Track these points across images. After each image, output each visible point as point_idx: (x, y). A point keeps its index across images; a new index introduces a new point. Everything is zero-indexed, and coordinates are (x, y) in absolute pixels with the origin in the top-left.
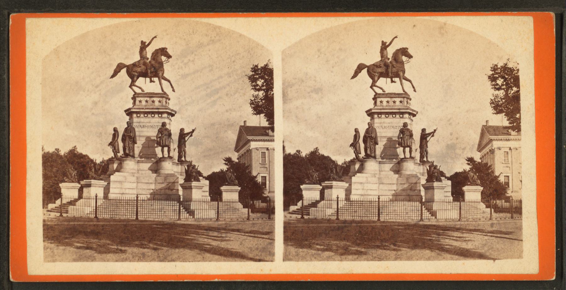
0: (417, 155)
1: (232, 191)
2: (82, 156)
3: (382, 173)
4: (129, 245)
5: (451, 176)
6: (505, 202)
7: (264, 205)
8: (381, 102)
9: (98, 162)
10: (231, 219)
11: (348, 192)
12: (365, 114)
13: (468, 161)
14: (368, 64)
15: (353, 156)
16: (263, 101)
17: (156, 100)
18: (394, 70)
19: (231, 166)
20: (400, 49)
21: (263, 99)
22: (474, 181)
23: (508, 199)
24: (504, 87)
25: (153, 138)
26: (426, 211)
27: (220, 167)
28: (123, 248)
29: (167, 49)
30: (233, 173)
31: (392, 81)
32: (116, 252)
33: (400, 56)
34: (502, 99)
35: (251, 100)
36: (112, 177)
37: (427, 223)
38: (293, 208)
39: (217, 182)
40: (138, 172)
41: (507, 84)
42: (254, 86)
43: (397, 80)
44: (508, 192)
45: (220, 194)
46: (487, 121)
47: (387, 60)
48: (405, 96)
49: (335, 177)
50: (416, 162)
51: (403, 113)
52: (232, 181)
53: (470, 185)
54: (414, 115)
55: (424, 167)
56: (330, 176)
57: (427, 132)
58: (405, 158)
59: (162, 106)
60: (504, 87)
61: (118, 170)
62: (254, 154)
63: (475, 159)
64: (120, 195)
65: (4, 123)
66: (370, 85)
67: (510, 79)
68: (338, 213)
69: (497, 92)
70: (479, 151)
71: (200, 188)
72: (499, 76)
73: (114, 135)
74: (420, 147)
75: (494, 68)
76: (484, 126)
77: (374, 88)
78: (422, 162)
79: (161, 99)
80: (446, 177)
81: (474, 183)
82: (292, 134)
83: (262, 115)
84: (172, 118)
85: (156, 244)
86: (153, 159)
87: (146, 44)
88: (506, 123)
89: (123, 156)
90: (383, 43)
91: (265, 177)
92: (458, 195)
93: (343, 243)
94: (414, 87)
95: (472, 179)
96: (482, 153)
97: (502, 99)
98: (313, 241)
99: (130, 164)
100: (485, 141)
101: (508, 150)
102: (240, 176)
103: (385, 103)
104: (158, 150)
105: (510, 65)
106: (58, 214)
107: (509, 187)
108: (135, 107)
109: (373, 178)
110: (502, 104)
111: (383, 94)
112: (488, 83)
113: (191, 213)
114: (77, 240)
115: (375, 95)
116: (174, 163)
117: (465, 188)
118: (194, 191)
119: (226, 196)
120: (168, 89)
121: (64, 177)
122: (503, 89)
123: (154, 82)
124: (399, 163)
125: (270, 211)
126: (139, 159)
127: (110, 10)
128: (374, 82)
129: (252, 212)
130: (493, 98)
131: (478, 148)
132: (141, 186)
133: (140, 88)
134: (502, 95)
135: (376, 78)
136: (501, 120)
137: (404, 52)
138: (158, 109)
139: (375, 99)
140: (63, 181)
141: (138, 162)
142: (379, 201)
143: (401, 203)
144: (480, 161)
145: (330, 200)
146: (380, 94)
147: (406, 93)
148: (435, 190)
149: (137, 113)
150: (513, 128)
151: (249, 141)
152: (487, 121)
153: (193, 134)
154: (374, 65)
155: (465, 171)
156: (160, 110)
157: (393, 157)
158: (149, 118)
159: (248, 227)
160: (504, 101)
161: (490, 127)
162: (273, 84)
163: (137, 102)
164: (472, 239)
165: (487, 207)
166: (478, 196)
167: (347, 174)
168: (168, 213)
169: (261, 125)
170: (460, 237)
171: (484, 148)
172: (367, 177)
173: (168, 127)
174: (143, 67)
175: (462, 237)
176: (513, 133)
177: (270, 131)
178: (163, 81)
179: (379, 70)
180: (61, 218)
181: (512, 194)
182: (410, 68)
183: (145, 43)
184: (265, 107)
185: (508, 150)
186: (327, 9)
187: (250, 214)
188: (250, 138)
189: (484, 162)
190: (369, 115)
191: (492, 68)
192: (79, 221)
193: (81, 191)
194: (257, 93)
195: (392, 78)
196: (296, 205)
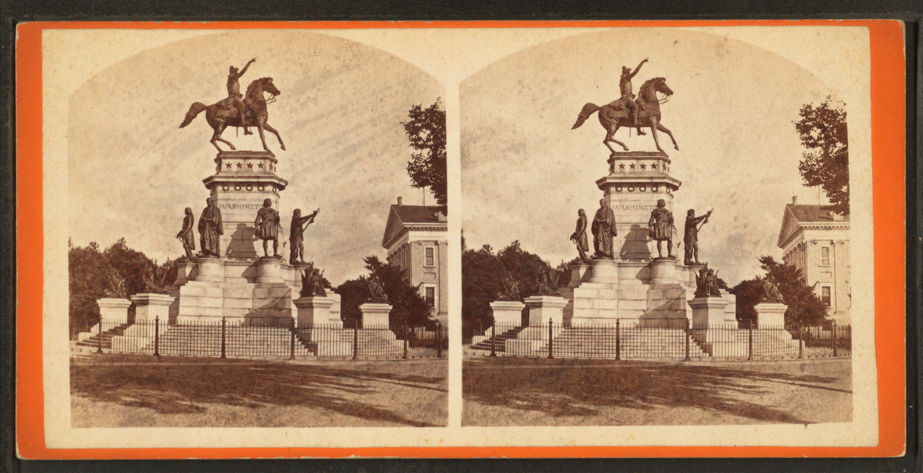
0: (680, 253)
1: (377, 312)
2: (133, 255)
3: (623, 282)
4: (211, 400)
5: (736, 288)
7: (430, 334)
8: (622, 166)
9: (160, 264)
10: (377, 358)
11: (568, 313)
12: (596, 186)
13: (763, 262)
14: (600, 105)
15: (575, 254)
17: (255, 163)
18: (643, 114)
19: (377, 271)
20: (653, 80)
21: (430, 162)
22: (773, 295)
23: (828, 325)
24: (822, 142)
25: (249, 225)
26: (694, 344)
27: (359, 272)
29: (272, 79)
30: (380, 282)
31: (640, 133)
33: (653, 91)
34: (818, 161)
35: (410, 164)
36: (182, 288)
37: (696, 363)
38: (477, 339)
39: (353, 296)
40: (225, 281)
41: (827, 137)
42: (415, 140)
43: (647, 130)
44: (829, 313)
45: (359, 316)
46: (794, 198)
47: (631, 98)
48: (660, 156)
49: (547, 288)
50: (678, 263)
51: (657, 185)
52: (379, 295)
54: (676, 188)
55: (692, 272)
56: (538, 288)
57: (697, 215)
59: (265, 172)
60: (822, 142)
61: (193, 277)
62: (414, 252)
63: (775, 260)
64: (196, 319)
65: (7, 200)
66: (604, 138)
67: (832, 129)
68: (550, 348)
70: (782, 247)
71: (327, 306)
73: (186, 221)
74: (685, 240)
75: (806, 111)
76: (789, 205)
77: (610, 143)
78: (689, 265)
80: (727, 289)
81: (773, 299)
82: (477, 219)
83: (428, 188)
84: (281, 193)
85: (254, 398)
86: (249, 260)
87: (239, 72)
88: (825, 201)
89: (201, 254)
90: (625, 71)
91: (433, 288)
92: (747, 318)
93: (559, 397)
94: (674, 142)
95: (770, 291)
96: (786, 249)
97: (818, 161)
98: (511, 393)
99: (211, 268)
101: (828, 244)
102: (392, 287)
103: (627, 169)
105: (832, 107)
106: (95, 350)
107: (829, 304)
108: (220, 174)
109: (609, 291)
110: (426, 172)
111: (625, 154)
113: (312, 347)
114: (125, 392)
115: (611, 156)
116: (283, 266)
117: (759, 307)
118: (316, 311)
119: (368, 320)
120: (273, 146)
121: (105, 288)
122: (821, 145)
123: (251, 133)
125: (440, 345)
126: (227, 259)
127: (180, 17)
128: (610, 134)
129: (412, 346)
130: (803, 160)
131: (782, 236)
132: (230, 303)
133: (228, 143)
134: (818, 155)
135: (613, 128)
136: (817, 196)
137: (659, 84)
138: (258, 177)
139: (611, 161)
140: (104, 296)
141: (226, 264)
142: (618, 328)
143: (655, 332)
144: (783, 262)
145: (539, 327)
146: (619, 154)
147: (662, 152)
148: (710, 311)
149: (223, 184)
150: (837, 210)
151: (406, 230)
152: (794, 198)
154: (609, 105)
156: (261, 180)
157: (641, 256)
158: (243, 192)
159: (404, 369)
160: (821, 164)
162: (444, 137)
163: (224, 167)
164: (770, 390)
165: (794, 338)
166: (780, 320)
167: (566, 284)
168: (273, 347)
169: (426, 205)
170: (750, 387)
171: (789, 241)
172: (598, 289)
173: (273, 206)
174: (233, 109)
175: (753, 387)
176: (837, 217)
177: (440, 213)
178: (266, 132)
179: (619, 114)
180: (99, 355)
181: (835, 317)
182: (669, 111)
183: (237, 69)
184: (432, 175)
185: (828, 244)
187: (408, 349)
188: (407, 224)
190: (601, 188)
191: (802, 111)
193: (132, 311)
194: (419, 151)
195: (638, 128)
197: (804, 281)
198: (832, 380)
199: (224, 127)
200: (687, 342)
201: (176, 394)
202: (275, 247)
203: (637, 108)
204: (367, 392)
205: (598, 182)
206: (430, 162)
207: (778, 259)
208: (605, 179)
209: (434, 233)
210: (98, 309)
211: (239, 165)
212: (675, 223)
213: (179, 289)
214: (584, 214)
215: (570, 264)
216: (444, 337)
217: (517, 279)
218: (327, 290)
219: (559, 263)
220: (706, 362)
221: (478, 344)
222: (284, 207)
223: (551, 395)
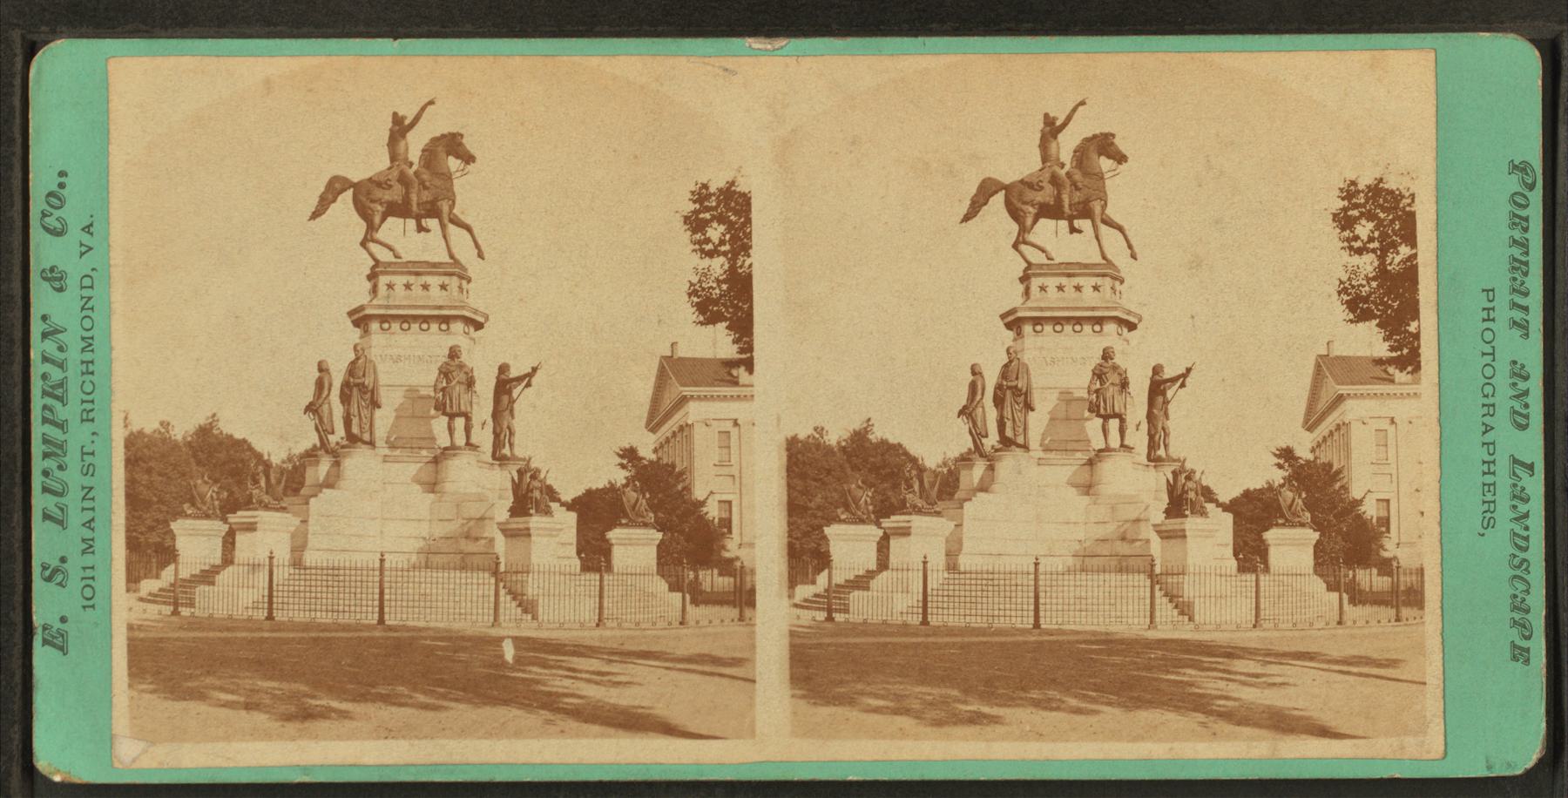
2: (886, 447)
4: (1010, 701)
5: (1234, 502)
6: (720, 574)
7: (724, 583)
8: (390, 286)
9: (276, 460)
11: (299, 547)
12: (1001, 324)
13: (622, 457)
14: (1007, 181)
15: (312, 439)
16: (724, 287)
21: (724, 281)
22: (1295, 514)
23: (1386, 567)
24: (1376, 245)
25: (423, 392)
26: (1165, 600)
27: (1264, 473)
28: (344, 706)
29: (1113, 136)
30: (1298, 491)
32: (975, 719)
34: (1368, 279)
35: (692, 284)
38: (149, 586)
39: (598, 514)
41: (1383, 237)
42: (699, 242)
43: (432, 223)
45: (1262, 551)
47: (1057, 169)
48: (454, 269)
49: (266, 499)
51: (446, 320)
53: (626, 525)
55: (506, 473)
56: (904, 501)
58: (1108, 449)
60: (1376, 245)
61: (984, 488)
67: (1392, 222)
68: (270, 602)
69: (1356, 260)
71: (551, 533)
72: (1362, 214)
75: (1349, 192)
78: (499, 458)
80: (1219, 505)
82: (805, 384)
83: (721, 326)
85: (1084, 697)
86: (424, 453)
87: (407, 122)
88: (1382, 349)
89: (345, 442)
93: (936, 692)
94: (1130, 247)
95: (634, 507)
96: (659, 434)
97: (1368, 279)
98: (859, 686)
99: (358, 463)
100: (667, 402)
101: (728, 426)
102: (659, 500)
104: (439, 425)
105: (1391, 184)
106: (168, 610)
110: (1369, 296)
112: (685, 236)
113: (528, 607)
114: (218, 683)
115: (373, 268)
117: (614, 535)
119: (620, 556)
120: (465, 251)
121: (187, 502)
122: (725, 254)
123: (428, 231)
124: (436, 461)
125: (743, 598)
126: (387, 452)
127: (305, 30)
128: (1023, 230)
130: (695, 280)
131: (1306, 421)
134: (1370, 268)
135: (1029, 221)
136: (1369, 341)
139: (372, 276)
140: (182, 514)
141: (385, 459)
142: (382, 569)
143: (440, 575)
144: (1311, 457)
145: (895, 571)
146: (1041, 266)
147: (456, 262)
150: (1401, 363)
153: (534, 380)
154: (1022, 181)
159: (689, 643)
160: (1374, 284)
162: (749, 236)
163: (382, 289)
164: (1291, 681)
165: (671, 589)
166: (1307, 559)
167: (296, 491)
170: (1257, 676)
171: (668, 415)
173: (464, 358)
175: (608, 673)
176: (1400, 376)
177: (742, 369)
180: (829, 625)
181: (1399, 553)
182: (1123, 191)
184: (729, 302)
185: (728, 426)
186: (906, 26)
187: (689, 608)
189: (1323, 459)
192: (201, 628)
193: (229, 542)
194: (707, 262)
196: (814, 582)
197: (687, 489)
198: (1393, 663)
200: (1152, 597)
201: (955, 693)
202: (468, 430)
203: (1065, 190)
205: (1003, 317)
208: (362, 308)
209: (735, 405)
210: (173, 538)
211: (408, 286)
213: (307, 503)
214: (327, 371)
215: (302, 457)
216: (748, 586)
217: (871, 486)
218: (554, 506)
219: (284, 456)
220: (1186, 633)
221: (806, 600)
222: (483, 365)
223: (275, 684)
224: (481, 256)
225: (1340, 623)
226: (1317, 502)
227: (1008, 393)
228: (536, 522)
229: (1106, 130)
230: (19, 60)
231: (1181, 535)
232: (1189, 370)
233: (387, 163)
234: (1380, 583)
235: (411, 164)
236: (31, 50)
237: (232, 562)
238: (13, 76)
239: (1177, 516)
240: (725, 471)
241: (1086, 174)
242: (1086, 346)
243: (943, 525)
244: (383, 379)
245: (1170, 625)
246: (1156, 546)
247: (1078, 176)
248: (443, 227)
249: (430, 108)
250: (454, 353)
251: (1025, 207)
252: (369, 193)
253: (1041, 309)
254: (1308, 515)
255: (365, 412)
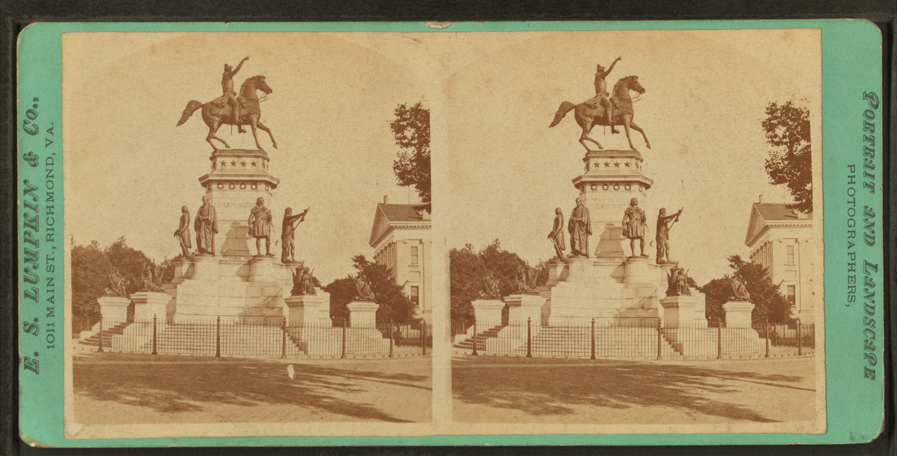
4: (577, 401)
5: (706, 287)
6: (412, 328)
7: (414, 333)
8: (223, 164)
9: (158, 263)
10: (741, 357)
11: (171, 312)
12: (573, 185)
14: (576, 103)
15: (179, 251)
16: (414, 164)
21: (414, 161)
22: (741, 294)
23: (793, 324)
24: (787, 140)
25: (242, 224)
26: (666, 343)
27: (723, 270)
29: (637, 77)
30: (742, 281)
31: (614, 131)
32: (558, 411)
33: (626, 89)
34: (783, 160)
35: (396, 162)
38: (85, 335)
42: (400, 139)
43: (247, 128)
45: (722, 315)
47: (605, 96)
48: (260, 154)
49: (152, 285)
53: (358, 300)
55: (289, 270)
56: (517, 286)
60: (787, 140)
63: (367, 259)
66: (206, 136)
67: (796, 127)
68: (155, 344)
71: (315, 304)
72: (779, 122)
73: (183, 220)
78: (286, 262)
79: (255, 160)
80: (697, 288)
82: (461, 219)
83: (413, 186)
85: (620, 399)
86: (243, 259)
87: (233, 70)
88: (791, 200)
89: (197, 253)
94: (646, 141)
95: (362, 290)
96: (377, 248)
97: (783, 160)
98: (492, 392)
99: (205, 265)
100: (382, 230)
101: (417, 243)
102: (377, 286)
104: (251, 243)
105: (796, 105)
106: (96, 348)
110: (783, 169)
112: (392, 135)
113: (302, 347)
117: (351, 306)
119: (354, 318)
120: (266, 144)
121: (107, 287)
122: (415, 145)
123: (245, 132)
124: (249, 263)
125: (425, 342)
127: (174, 17)
128: (585, 131)
129: (774, 344)
130: (398, 160)
131: (747, 241)
133: (223, 142)
134: (784, 153)
135: (589, 126)
136: (783, 195)
138: (252, 176)
139: (213, 158)
141: (221, 262)
142: (218, 325)
144: (750, 261)
145: (512, 326)
146: (595, 152)
147: (261, 150)
150: (801, 208)
153: (306, 217)
154: (584, 104)
155: (350, 279)
157: (242, 253)
159: (394, 367)
160: (786, 162)
161: (390, 205)
162: (428, 135)
163: (219, 165)
165: (384, 337)
166: (747, 319)
167: (169, 281)
170: (719, 386)
171: (382, 237)
173: (266, 204)
174: (228, 107)
175: (348, 385)
177: (425, 211)
180: (474, 357)
181: (800, 316)
182: (642, 109)
184: (417, 173)
185: (417, 243)
187: (394, 347)
189: (757, 262)
191: (396, 110)
193: (131, 309)
194: (404, 150)
195: (239, 125)
196: (465, 333)
197: (393, 279)
199: (219, 126)
202: (268, 245)
204: (354, 390)
206: (414, 161)
207: (370, 259)
208: (207, 176)
210: (99, 307)
212: (647, 222)
213: (176, 288)
214: (187, 212)
215: (547, 263)
216: (428, 335)
218: (317, 289)
219: (162, 260)
220: (678, 362)
221: (461, 343)
222: (276, 209)
224: (275, 146)
225: (766, 356)
226: (753, 287)
227: (577, 224)
228: (306, 298)
229: (633, 74)
230: (11, 34)
231: (676, 306)
232: (680, 212)
233: (220, 93)
234: (790, 333)
235: (235, 94)
236: (18, 29)
237: (133, 321)
238: (7, 43)
239: (673, 295)
240: (415, 269)
241: (621, 99)
242: (622, 198)
243: (540, 300)
244: (219, 216)
245: (669, 357)
246: (661, 312)
247: (617, 101)
248: (253, 129)
249: (246, 62)
250: (259, 202)
251: (586, 118)
252: (584, 111)
253: (596, 177)
254: (748, 294)
255: (209, 236)
